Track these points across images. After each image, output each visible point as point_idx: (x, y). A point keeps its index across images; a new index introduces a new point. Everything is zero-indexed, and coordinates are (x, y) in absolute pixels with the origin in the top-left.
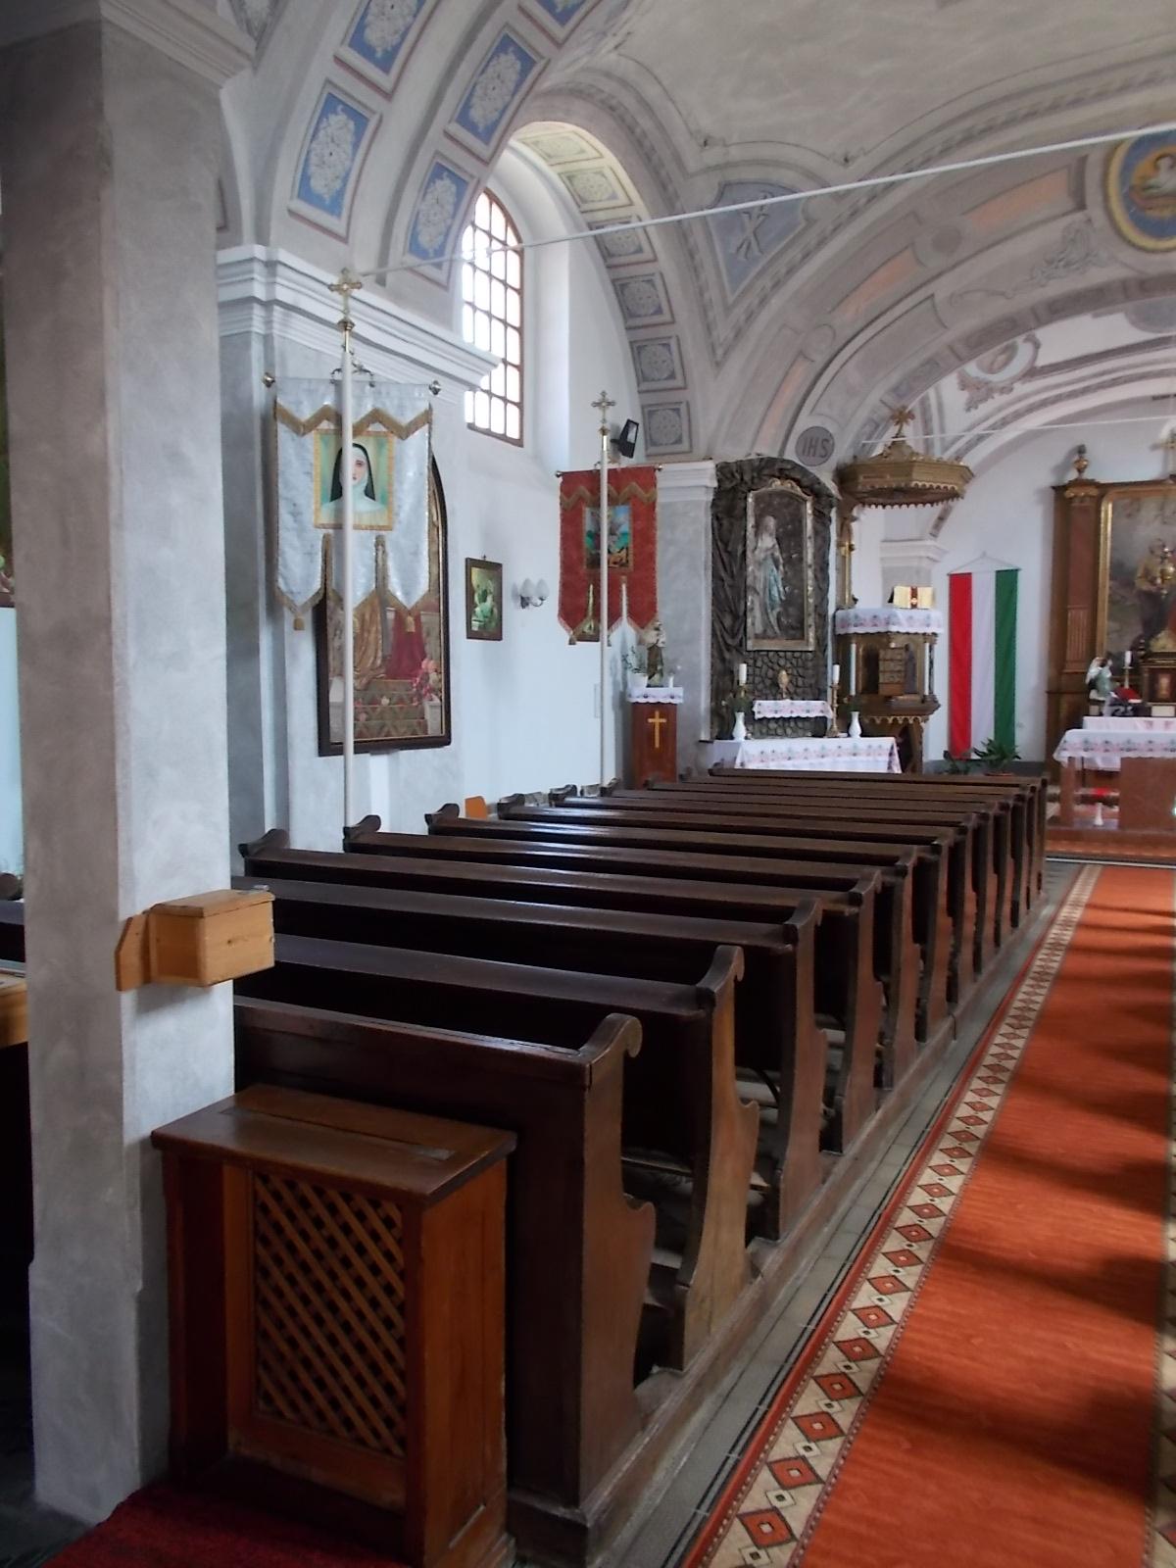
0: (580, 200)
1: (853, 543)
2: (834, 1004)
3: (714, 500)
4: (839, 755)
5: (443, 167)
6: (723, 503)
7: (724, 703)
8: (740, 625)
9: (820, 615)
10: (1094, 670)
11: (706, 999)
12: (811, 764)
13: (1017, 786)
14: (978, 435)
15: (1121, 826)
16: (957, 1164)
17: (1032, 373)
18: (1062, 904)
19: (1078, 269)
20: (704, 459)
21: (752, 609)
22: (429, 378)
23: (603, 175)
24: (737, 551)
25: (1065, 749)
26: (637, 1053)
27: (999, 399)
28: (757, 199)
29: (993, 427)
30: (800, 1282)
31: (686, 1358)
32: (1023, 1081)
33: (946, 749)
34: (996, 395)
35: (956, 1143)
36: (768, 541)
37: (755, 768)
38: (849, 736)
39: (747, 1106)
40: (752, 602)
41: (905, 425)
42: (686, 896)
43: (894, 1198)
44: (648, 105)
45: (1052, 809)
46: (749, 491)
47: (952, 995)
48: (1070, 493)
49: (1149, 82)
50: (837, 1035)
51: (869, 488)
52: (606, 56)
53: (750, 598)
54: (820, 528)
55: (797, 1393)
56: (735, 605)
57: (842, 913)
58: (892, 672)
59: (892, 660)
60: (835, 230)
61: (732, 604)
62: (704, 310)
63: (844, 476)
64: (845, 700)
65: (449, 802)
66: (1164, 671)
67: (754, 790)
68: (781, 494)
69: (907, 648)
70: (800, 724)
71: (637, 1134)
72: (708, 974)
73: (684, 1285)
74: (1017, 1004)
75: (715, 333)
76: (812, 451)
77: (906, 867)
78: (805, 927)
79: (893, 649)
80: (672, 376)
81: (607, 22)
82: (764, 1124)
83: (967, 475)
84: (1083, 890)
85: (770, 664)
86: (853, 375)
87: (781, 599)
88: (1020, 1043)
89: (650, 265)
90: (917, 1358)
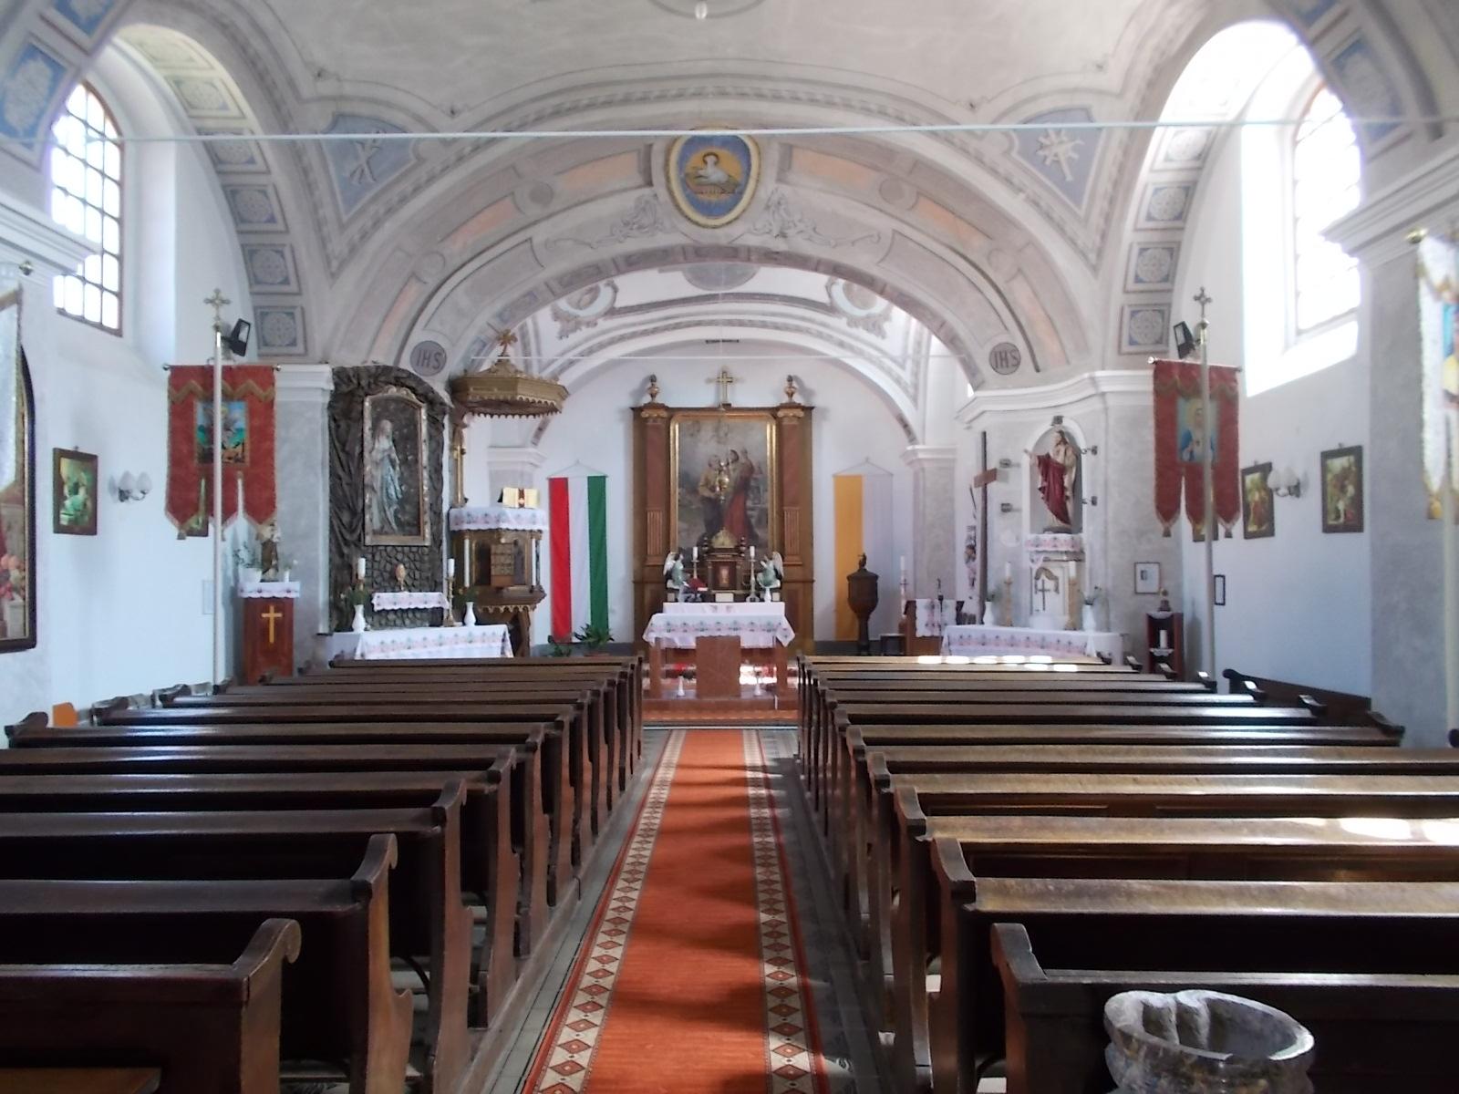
0: (189, 105)
1: (464, 447)
2: (478, 883)
4: (457, 643)
5: (36, 49)
6: (340, 405)
7: (342, 596)
8: (358, 521)
9: (435, 513)
10: (669, 563)
11: (364, 891)
12: (430, 653)
14: (570, 360)
15: (698, 695)
17: (612, 312)
18: (657, 767)
19: (647, 232)
20: (321, 363)
21: (370, 506)
22: (19, 259)
23: (215, 87)
24: (354, 451)
25: (652, 631)
26: (296, 957)
27: (585, 332)
28: (369, 132)
32: (642, 929)
33: (550, 634)
34: (583, 328)
35: (589, 998)
36: (385, 443)
37: (375, 658)
40: (370, 500)
41: (508, 346)
42: (323, 789)
43: (537, 1062)
45: (646, 682)
46: (367, 395)
47: (575, 859)
48: (645, 414)
50: (480, 911)
51: (478, 398)
53: (368, 496)
54: (433, 431)
56: (353, 502)
57: (482, 791)
59: (502, 554)
60: (443, 170)
62: (319, 225)
63: (456, 386)
65: (34, 711)
66: (725, 564)
67: (377, 679)
68: (398, 400)
69: (516, 543)
70: (418, 615)
72: (363, 862)
74: (629, 860)
76: (1004, 363)
77: (536, 743)
78: (452, 808)
79: (503, 544)
82: (418, 1014)
83: (563, 393)
84: (673, 753)
85: (389, 559)
86: (461, 297)
87: (397, 497)
88: (635, 895)
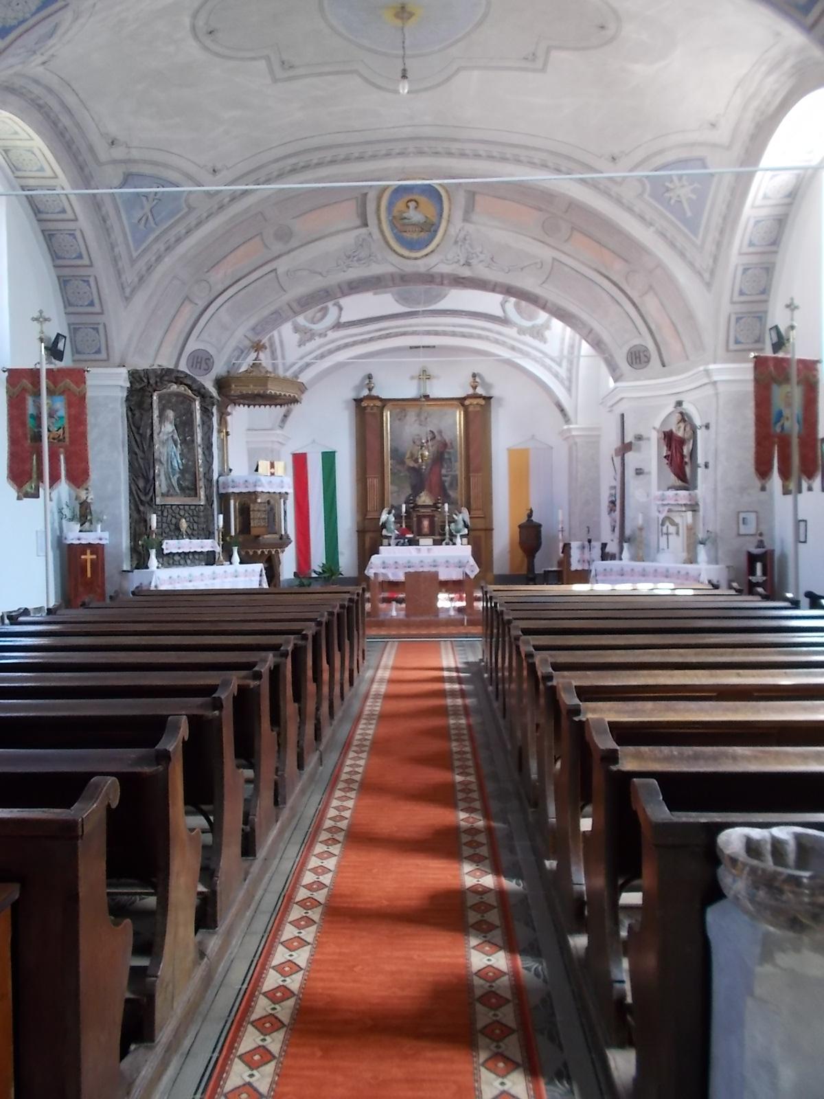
1: (228, 430)
2: (247, 753)
3: (127, 396)
4: (226, 577)
6: (135, 398)
7: (140, 542)
9: (208, 480)
10: (384, 517)
11: (165, 757)
12: (206, 585)
13: (348, 592)
15: (407, 615)
16: (332, 849)
17: (338, 326)
18: (377, 668)
20: (119, 366)
21: (159, 475)
24: (146, 432)
25: (371, 568)
27: (318, 341)
29: (316, 358)
30: (232, 956)
31: (156, 1032)
32: (368, 787)
34: (317, 338)
36: (169, 428)
38: (231, 563)
39: (194, 833)
40: (159, 471)
44: (68, 108)
45: (368, 606)
46: (155, 391)
48: (364, 404)
49: (401, 154)
50: (249, 773)
52: (34, 67)
53: (157, 467)
55: (240, 1037)
56: (146, 472)
57: (249, 686)
58: (259, 519)
61: (144, 471)
62: (115, 260)
63: (221, 384)
64: (228, 538)
66: (425, 516)
68: (178, 395)
69: (269, 502)
70: (197, 557)
71: (117, 871)
73: (153, 977)
75: (124, 278)
78: (227, 698)
80: (92, 304)
81: (36, 43)
82: (205, 847)
83: (302, 388)
86: (224, 316)
87: (179, 469)
88: (362, 762)
89: (71, 223)
90: (320, 991)
